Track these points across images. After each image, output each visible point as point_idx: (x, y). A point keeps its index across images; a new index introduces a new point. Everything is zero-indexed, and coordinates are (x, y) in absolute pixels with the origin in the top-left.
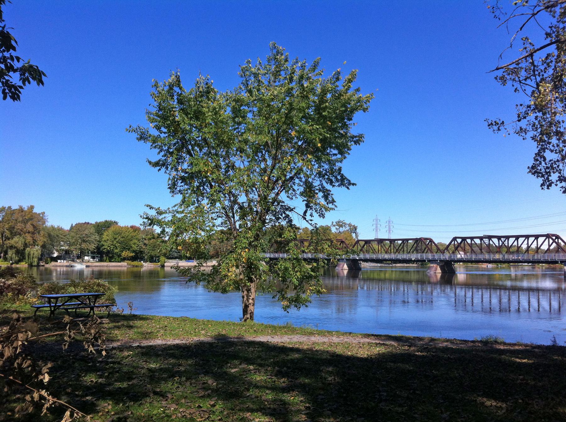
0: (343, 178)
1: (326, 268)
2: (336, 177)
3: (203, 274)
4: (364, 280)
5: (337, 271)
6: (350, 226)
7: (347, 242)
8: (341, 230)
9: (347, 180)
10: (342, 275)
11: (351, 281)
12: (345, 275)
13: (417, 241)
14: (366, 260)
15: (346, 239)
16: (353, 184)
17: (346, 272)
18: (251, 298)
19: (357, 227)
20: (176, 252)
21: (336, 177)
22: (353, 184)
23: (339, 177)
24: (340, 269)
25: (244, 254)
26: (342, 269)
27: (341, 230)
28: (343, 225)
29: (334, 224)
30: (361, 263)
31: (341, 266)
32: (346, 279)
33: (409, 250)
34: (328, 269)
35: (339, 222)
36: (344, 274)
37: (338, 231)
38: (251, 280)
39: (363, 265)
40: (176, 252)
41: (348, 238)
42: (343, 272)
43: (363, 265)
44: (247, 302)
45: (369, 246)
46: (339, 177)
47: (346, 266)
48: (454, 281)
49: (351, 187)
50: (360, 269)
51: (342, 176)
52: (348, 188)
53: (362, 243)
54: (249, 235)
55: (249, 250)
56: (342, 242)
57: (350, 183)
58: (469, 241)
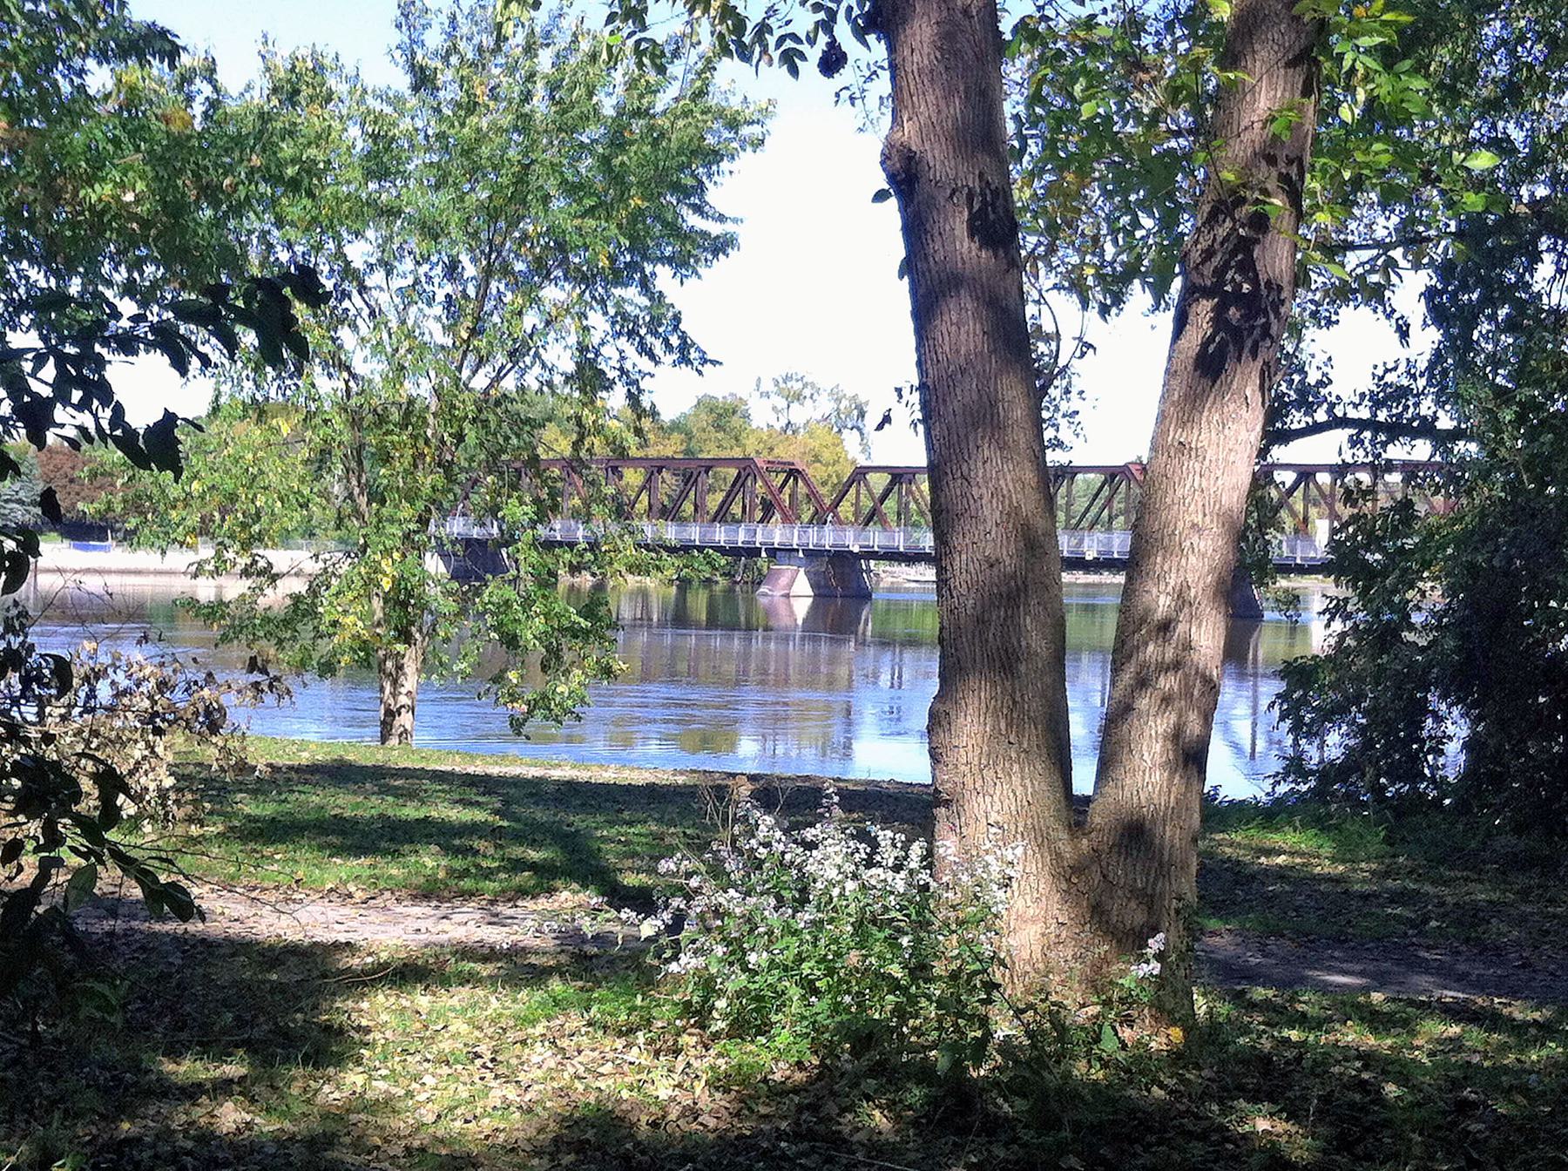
0: (685, 345)
1: (718, 588)
2: (666, 342)
3: (267, 620)
4: (885, 642)
5: (763, 601)
6: (839, 401)
7: (815, 473)
8: (799, 414)
9: (698, 349)
10: (785, 621)
11: (824, 649)
12: (800, 622)
13: (1113, 476)
14: (892, 556)
15: (817, 459)
16: (714, 363)
17: (802, 608)
18: (403, 690)
19: (867, 403)
20: (20, 502)
21: (666, 342)
22: (714, 363)
23: (674, 341)
24: (778, 593)
25: (386, 565)
26: (787, 596)
27: (799, 414)
28: (807, 392)
29: (768, 385)
30: (869, 571)
31: (783, 581)
32: (803, 638)
33: (1074, 521)
34: (730, 591)
35: (787, 379)
36: (792, 613)
37: (783, 422)
38: (405, 636)
39: (892, 574)
40: (20, 502)
41: (827, 455)
42: (790, 606)
43: (892, 574)
44: (391, 701)
45: (909, 492)
46: (674, 341)
47: (803, 585)
48: (1256, 651)
49: (707, 369)
50: (865, 596)
51: (683, 337)
52: (700, 373)
53: (879, 482)
54: (402, 515)
55: (404, 556)
56: (794, 473)
57: (704, 361)
58: (1324, 478)
